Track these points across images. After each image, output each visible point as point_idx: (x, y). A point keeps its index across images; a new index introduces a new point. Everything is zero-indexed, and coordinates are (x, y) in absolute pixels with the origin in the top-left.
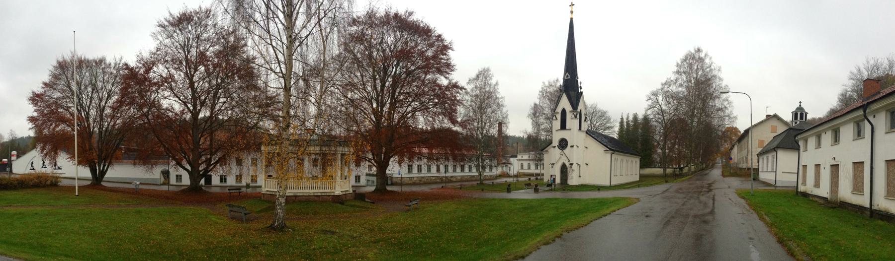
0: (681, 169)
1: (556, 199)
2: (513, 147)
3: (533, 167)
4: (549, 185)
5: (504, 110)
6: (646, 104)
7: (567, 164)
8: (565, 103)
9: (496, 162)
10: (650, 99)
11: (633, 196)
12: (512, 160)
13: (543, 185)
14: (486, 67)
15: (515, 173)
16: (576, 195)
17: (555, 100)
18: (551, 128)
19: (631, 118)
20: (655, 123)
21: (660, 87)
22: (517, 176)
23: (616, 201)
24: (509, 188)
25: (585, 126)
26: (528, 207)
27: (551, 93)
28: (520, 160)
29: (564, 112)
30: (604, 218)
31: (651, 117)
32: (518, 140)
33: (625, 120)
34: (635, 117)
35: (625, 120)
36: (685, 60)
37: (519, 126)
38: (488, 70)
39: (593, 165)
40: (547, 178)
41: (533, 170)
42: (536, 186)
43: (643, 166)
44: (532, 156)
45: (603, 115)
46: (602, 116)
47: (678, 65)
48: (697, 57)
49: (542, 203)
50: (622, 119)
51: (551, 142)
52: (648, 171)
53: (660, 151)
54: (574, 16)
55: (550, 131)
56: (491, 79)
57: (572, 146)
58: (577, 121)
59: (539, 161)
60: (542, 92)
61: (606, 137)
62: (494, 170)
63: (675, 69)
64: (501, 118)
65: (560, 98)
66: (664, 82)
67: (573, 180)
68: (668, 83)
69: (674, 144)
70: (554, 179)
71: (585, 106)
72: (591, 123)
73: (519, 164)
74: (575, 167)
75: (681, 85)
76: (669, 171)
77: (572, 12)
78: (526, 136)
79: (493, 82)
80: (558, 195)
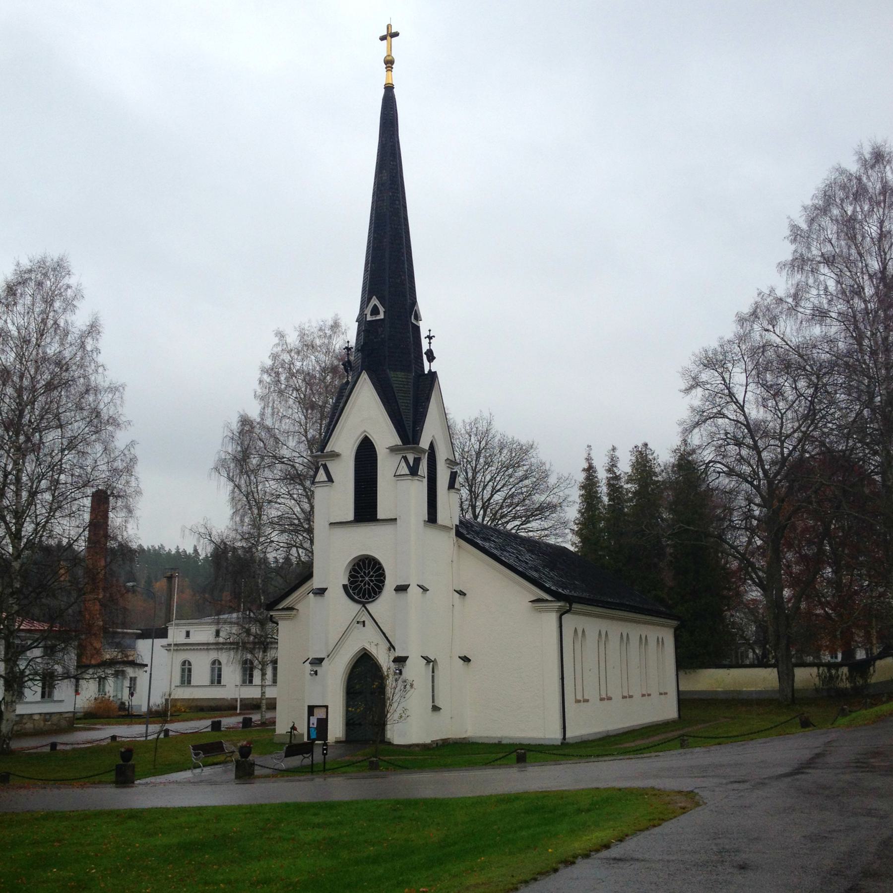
0: (861, 669)
1: (330, 806)
2: (150, 594)
3: (232, 674)
4: (295, 748)
5: (121, 440)
6: (683, 406)
7: (384, 659)
8: (367, 414)
9: (71, 659)
10: (696, 383)
11: (669, 784)
12: (143, 647)
13: (271, 745)
14: (54, 254)
15: (157, 700)
16: (427, 785)
17: (326, 402)
18: (309, 516)
19: (625, 467)
20: (725, 482)
21: (730, 330)
23: (604, 803)
24: (125, 766)
25: (450, 508)
26: (205, 839)
27: (309, 378)
28: (178, 647)
29: (366, 454)
30: (565, 873)
31: (708, 455)
32: (172, 565)
33: (602, 475)
34: (643, 462)
35: (602, 475)
36: (824, 210)
37: (177, 509)
38: (59, 268)
39: (496, 667)
40: (289, 719)
41: (232, 687)
42: (245, 752)
43: (688, 659)
44: (229, 632)
45: (517, 457)
46: (515, 465)
47: (796, 234)
48: (873, 185)
49: (269, 820)
50: (590, 470)
51: (305, 572)
53: (754, 594)
54: (398, 78)
56: (69, 305)
57: (402, 589)
58: (418, 489)
59: (256, 649)
60: (271, 371)
61: (534, 546)
62: (63, 691)
63: (787, 251)
64: (102, 473)
65: (343, 395)
66: (746, 309)
67: (410, 723)
68: (764, 312)
69: (814, 564)
70: (323, 724)
71: (449, 428)
72: (474, 496)
73: (175, 666)
74: (415, 670)
75: (820, 315)
76: (805, 676)
77: (389, 63)
78: (205, 550)
79: (78, 320)
80: (340, 789)
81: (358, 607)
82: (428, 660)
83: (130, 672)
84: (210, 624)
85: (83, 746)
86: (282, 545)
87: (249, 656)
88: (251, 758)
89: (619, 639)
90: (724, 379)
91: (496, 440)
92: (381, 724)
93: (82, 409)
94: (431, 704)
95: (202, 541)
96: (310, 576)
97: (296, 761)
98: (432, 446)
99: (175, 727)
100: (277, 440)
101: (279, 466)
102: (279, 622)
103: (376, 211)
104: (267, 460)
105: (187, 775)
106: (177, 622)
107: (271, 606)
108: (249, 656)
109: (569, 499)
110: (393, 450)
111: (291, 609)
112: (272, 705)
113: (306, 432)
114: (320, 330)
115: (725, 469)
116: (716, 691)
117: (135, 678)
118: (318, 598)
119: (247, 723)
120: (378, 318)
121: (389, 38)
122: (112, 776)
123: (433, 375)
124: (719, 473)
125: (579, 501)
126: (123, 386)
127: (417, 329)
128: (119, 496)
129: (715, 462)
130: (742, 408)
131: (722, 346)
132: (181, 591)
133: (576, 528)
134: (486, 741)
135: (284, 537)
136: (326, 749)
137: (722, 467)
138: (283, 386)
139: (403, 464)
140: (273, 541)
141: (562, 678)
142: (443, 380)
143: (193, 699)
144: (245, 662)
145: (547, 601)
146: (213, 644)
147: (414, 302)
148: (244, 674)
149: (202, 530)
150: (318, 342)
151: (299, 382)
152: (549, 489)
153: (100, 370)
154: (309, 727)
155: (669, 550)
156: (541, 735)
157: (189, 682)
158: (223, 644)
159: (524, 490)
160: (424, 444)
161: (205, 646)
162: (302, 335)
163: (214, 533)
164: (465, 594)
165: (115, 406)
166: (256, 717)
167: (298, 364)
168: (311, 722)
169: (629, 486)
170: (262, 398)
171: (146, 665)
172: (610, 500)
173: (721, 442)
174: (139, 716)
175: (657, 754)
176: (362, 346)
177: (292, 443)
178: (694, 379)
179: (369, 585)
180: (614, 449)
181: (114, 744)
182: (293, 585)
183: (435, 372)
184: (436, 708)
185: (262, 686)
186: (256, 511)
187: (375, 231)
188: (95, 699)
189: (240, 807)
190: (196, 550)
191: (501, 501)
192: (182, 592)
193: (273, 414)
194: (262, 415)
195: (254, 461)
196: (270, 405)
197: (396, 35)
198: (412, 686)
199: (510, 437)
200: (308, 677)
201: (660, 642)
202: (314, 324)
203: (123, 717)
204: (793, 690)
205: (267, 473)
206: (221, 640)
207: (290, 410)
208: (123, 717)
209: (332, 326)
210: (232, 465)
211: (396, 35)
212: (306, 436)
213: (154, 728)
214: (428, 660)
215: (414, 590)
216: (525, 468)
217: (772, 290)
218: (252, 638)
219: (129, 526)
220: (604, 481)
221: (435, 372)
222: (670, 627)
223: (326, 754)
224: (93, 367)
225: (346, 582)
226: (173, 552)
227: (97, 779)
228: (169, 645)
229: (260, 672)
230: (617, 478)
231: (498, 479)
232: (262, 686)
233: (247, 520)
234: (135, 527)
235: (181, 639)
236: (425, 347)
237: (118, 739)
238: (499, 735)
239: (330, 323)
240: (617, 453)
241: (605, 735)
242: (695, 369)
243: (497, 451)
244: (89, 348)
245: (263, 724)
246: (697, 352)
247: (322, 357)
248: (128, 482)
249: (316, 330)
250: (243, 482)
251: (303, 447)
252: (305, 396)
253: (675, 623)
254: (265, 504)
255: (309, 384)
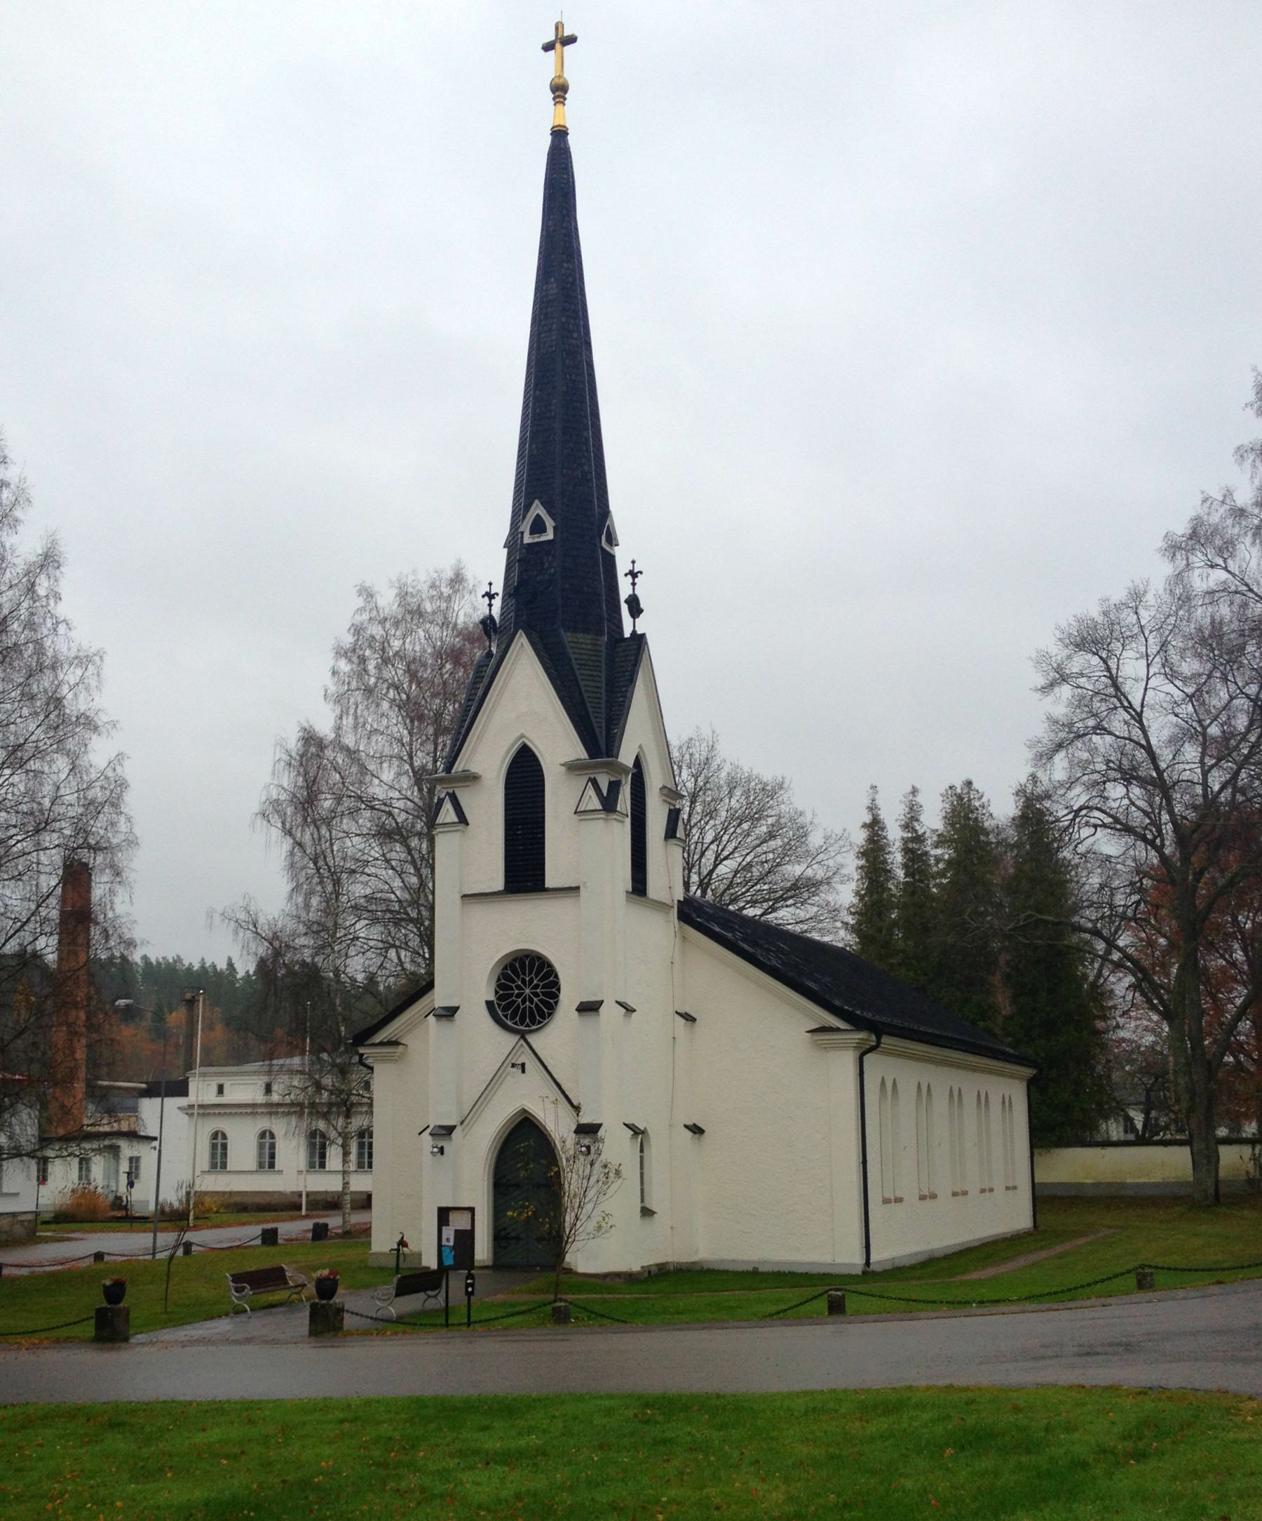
3: (292, 1152)
5: (99, 753)
7: (559, 1126)
8: (526, 707)
10: (1061, 677)
12: (149, 1108)
15: (172, 1196)
19: (933, 820)
22: (172, 1218)
24: (111, 1314)
28: (206, 1110)
29: (524, 774)
32: (186, 986)
33: (894, 834)
34: (964, 813)
35: (894, 834)
37: (200, 884)
39: (749, 1142)
41: (293, 1174)
42: (326, 1288)
43: (1051, 1127)
45: (759, 801)
50: (875, 826)
52: (1076, 1165)
54: (573, 115)
55: (415, 917)
57: (589, 1008)
59: (336, 1112)
60: (352, 653)
66: (1181, 528)
67: (605, 1242)
70: (465, 1239)
73: (198, 1142)
74: (616, 1146)
76: (1233, 1159)
77: (560, 90)
81: (509, 1040)
82: (636, 1131)
83: (128, 1150)
84: (255, 1073)
85: (47, 1269)
86: (372, 943)
87: (321, 1125)
88: (337, 1300)
89: (915, 1094)
90: (1108, 669)
91: (723, 774)
92: (556, 1242)
93: (32, 697)
94: (639, 1205)
95: (241, 935)
96: (430, 985)
97: (413, 1302)
98: (637, 763)
99: (202, 1238)
100: (363, 770)
101: (368, 814)
102: (377, 1068)
103: (539, 348)
104: (347, 803)
105: (223, 1326)
106: (204, 1069)
107: (363, 1037)
108: (321, 1125)
109: (844, 871)
110: (573, 767)
111: (394, 1043)
112: (365, 1202)
113: (411, 757)
114: (433, 586)
115: (1108, 820)
116: (1082, 1184)
117: (138, 1159)
118: (445, 1024)
119: (320, 1232)
120: (544, 538)
121: (558, 46)
122: (89, 1329)
123: (639, 640)
124: (1095, 826)
125: (856, 877)
126: (101, 654)
127: (610, 561)
128: (100, 849)
129: (1090, 808)
130: (1139, 717)
131: (1106, 614)
132: (209, 1027)
133: (851, 920)
134: (731, 1267)
135: (376, 932)
136: (472, 1285)
137: (1102, 816)
138: (372, 680)
139: (591, 792)
140: (358, 938)
141: (864, 1162)
142: (657, 649)
143: (231, 1193)
144: (313, 1134)
145: (838, 1030)
146: (261, 1105)
147: (606, 513)
148: (312, 1155)
149: (242, 916)
150: (428, 607)
151: (397, 673)
152: (812, 856)
153: (62, 629)
154: (440, 1246)
155: (1003, 958)
156: (827, 1259)
157: (224, 1165)
158: (278, 1105)
159: (771, 856)
160: (626, 757)
161: (250, 1110)
162: (403, 595)
163: (262, 920)
164: (694, 1020)
165: (87, 689)
166: (334, 1222)
167: (396, 644)
168: (444, 1237)
169: (939, 851)
170: (339, 699)
171: (155, 1139)
172: (906, 875)
173: (1096, 777)
174: (144, 1219)
175: (1103, 1300)
176: (516, 589)
177: (388, 775)
178: (1058, 669)
179: (531, 1001)
180: (914, 791)
181: (100, 1266)
182: (391, 1008)
183: (643, 635)
184: (647, 1212)
185: (345, 1173)
186: (330, 888)
187: (536, 388)
188: (73, 1191)
189: (323, 1406)
190: (231, 965)
191: (730, 876)
192: (212, 1029)
193: (356, 727)
194: (338, 729)
195: (327, 803)
196: (352, 711)
197: (571, 40)
198: (618, 1173)
199: (746, 769)
200: (427, 1158)
201: (1006, 1104)
202: (422, 577)
203: (118, 1219)
204: (1217, 1182)
205: (347, 824)
206: (275, 1098)
207: (385, 722)
208: (118, 1219)
209: (452, 581)
210: (289, 811)
211: (571, 40)
212: (411, 765)
213: (167, 1238)
214: (636, 1131)
215: (609, 1011)
216: (770, 821)
217: (1228, 493)
218: (325, 1094)
219: (117, 900)
220: (898, 844)
221: (643, 635)
222: (1020, 1078)
223: (472, 1293)
224: (49, 625)
225: (492, 997)
226: (196, 967)
227: (64, 1333)
228: (191, 1107)
229: (340, 1150)
230: (919, 839)
231: (726, 838)
232: (345, 1173)
233: (315, 901)
234: (127, 899)
235: (211, 1097)
236: (625, 590)
237: (106, 1258)
238: (754, 1258)
239: (449, 574)
240: (920, 799)
241: (926, 1257)
242: (1058, 652)
243: (725, 790)
244: (42, 591)
245: (347, 1234)
246: (1063, 624)
247: (435, 631)
248: (113, 824)
249: (425, 587)
250: (307, 837)
251: (405, 782)
252: (408, 696)
253: (1029, 1072)
254: (344, 876)
255: (413, 676)
